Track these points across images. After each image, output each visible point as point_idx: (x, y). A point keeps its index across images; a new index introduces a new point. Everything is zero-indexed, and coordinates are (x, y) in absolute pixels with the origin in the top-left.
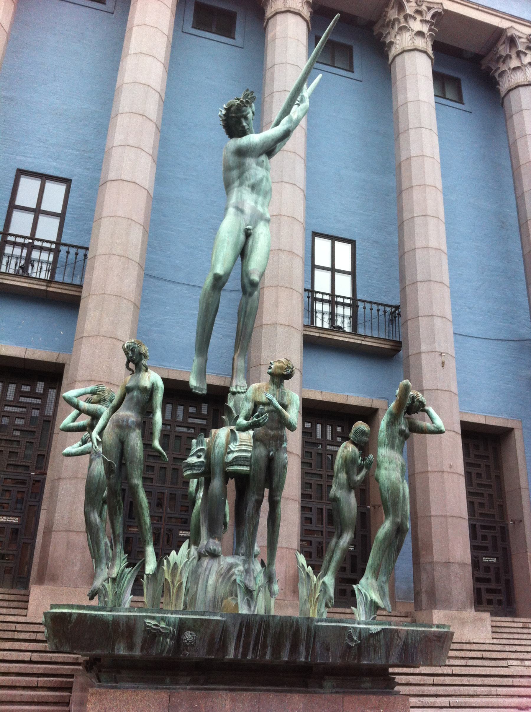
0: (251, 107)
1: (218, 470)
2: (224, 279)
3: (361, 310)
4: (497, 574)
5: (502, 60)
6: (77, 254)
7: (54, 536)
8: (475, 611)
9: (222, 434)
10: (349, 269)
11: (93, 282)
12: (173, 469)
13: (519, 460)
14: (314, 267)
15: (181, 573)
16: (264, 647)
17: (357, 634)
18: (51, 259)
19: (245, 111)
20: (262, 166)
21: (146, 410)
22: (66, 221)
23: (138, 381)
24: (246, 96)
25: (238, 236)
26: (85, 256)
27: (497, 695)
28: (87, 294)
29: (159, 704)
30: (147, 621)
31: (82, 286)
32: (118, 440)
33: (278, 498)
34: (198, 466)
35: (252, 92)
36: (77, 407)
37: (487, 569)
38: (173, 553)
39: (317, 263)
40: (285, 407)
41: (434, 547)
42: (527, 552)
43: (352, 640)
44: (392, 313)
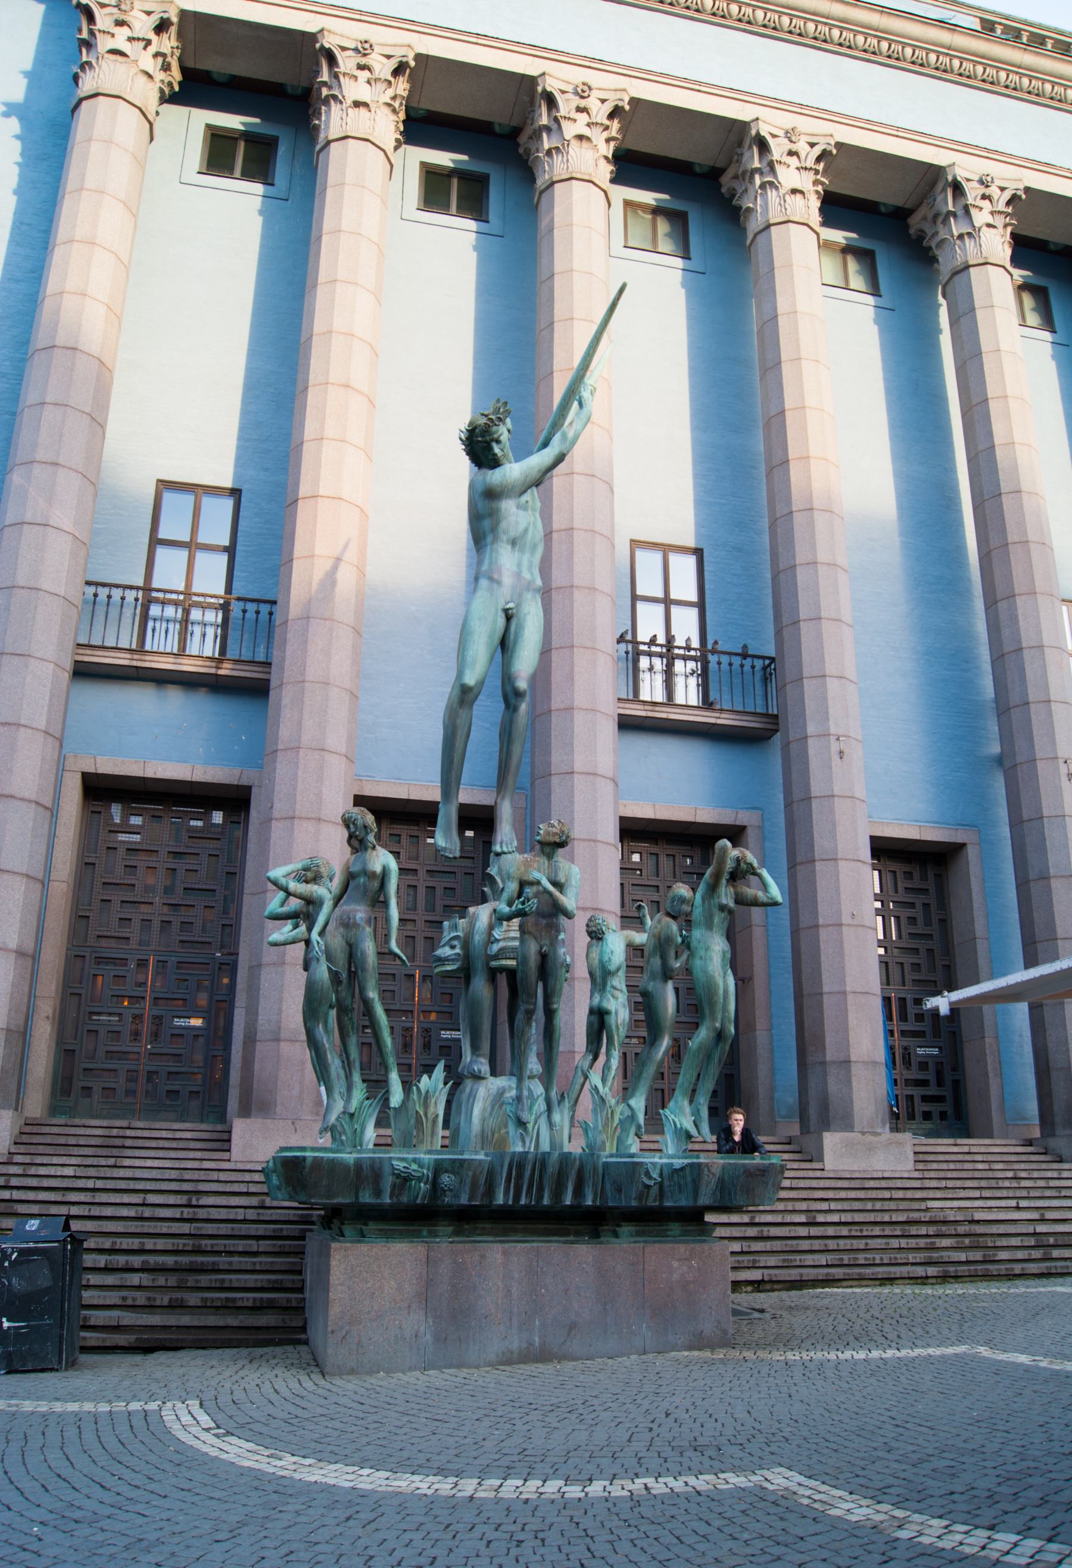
0: (504, 423)
1: (479, 965)
2: (475, 691)
3: (713, 666)
4: (939, 1074)
5: (940, 219)
6: (258, 612)
7: (259, 1046)
8: (892, 1130)
9: (483, 914)
10: (693, 597)
11: (287, 663)
12: (426, 938)
13: (974, 894)
14: (635, 598)
15: (436, 1103)
16: (541, 1189)
17: (658, 1171)
18: (220, 620)
19: (495, 433)
20: (525, 509)
21: (378, 901)
22: (237, 559)
23: (364, 863)
24: (497, 411)
25: (495, 622)
26: (271, 614)
27: (900, 1249)
28: (279, 683)
29: (416, 1260)
30: (395, 1163)
31: (270, 664)
32: (344, 944)
33: (555, 1006)
34: (453, 960)
35: (506, 403)
36: (286, 890)
37: (923, 1066)
38: (425, 1077)
39: (639, 592)
40: (558, 885)
41: (828, 1040)
42: (984, 1037)
43: (651, 1178)
44: (765, 668)
